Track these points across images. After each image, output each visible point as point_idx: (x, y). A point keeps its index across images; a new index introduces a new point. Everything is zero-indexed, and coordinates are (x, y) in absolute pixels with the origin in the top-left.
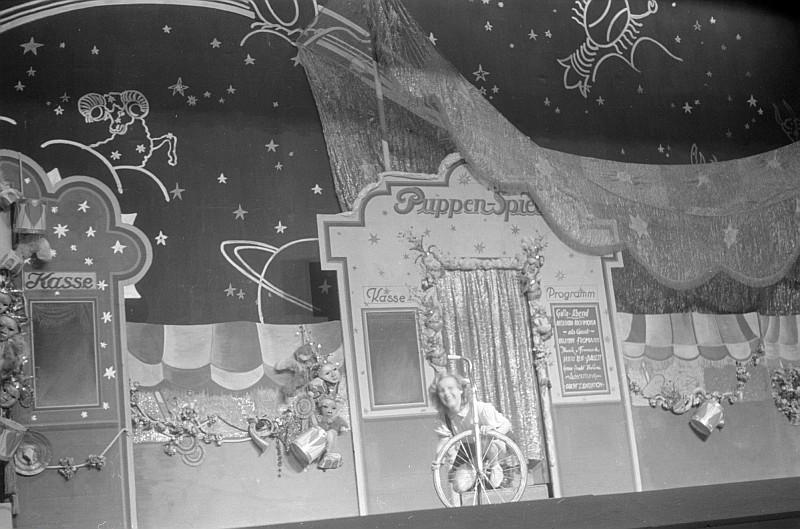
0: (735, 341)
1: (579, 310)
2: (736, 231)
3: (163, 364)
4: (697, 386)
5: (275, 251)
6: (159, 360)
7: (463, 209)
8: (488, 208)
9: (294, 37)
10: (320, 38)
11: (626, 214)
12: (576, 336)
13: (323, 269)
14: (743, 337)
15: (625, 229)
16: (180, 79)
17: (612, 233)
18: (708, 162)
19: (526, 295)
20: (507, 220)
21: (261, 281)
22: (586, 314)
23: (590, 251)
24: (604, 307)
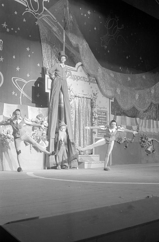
0: (134, 125)
1: (103, 112)
2: (138, 95)
3: (3, 115)
4: (125, 136)
5: (26, 82)
6: (2, 114)
7: (80, 79)
8: (86, 80)
9: (37, 15)
10: (43, 17)
11: (116, 87)
12: (102, 120)
13: (46, 91)
16: (5, 22)
17: (112, 92)
18: (130, 74)
19: (92, 107)
21: (22, 91)
22: (104, 114)
23: (107, 97)
24: (108, 112)
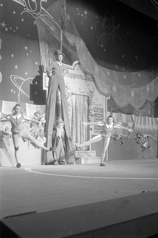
0: (130, 122)
3: (2, 112)
4: (121, 133)
5: (24, 80)
8: (83, 78)
10: (41, 17)
11: (112, 85)
12: (98, 117)
13: (44, 89)
14: (132, 122)
15: (112, 90)
16: (4, 22)
19: (89, 105)
20: (86, 82)
21: (20, 89)
22: (101, 111)
23: (103, 94)
24: (105, 110)
